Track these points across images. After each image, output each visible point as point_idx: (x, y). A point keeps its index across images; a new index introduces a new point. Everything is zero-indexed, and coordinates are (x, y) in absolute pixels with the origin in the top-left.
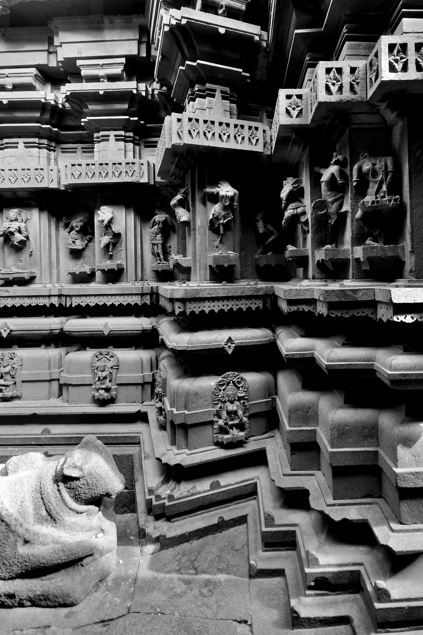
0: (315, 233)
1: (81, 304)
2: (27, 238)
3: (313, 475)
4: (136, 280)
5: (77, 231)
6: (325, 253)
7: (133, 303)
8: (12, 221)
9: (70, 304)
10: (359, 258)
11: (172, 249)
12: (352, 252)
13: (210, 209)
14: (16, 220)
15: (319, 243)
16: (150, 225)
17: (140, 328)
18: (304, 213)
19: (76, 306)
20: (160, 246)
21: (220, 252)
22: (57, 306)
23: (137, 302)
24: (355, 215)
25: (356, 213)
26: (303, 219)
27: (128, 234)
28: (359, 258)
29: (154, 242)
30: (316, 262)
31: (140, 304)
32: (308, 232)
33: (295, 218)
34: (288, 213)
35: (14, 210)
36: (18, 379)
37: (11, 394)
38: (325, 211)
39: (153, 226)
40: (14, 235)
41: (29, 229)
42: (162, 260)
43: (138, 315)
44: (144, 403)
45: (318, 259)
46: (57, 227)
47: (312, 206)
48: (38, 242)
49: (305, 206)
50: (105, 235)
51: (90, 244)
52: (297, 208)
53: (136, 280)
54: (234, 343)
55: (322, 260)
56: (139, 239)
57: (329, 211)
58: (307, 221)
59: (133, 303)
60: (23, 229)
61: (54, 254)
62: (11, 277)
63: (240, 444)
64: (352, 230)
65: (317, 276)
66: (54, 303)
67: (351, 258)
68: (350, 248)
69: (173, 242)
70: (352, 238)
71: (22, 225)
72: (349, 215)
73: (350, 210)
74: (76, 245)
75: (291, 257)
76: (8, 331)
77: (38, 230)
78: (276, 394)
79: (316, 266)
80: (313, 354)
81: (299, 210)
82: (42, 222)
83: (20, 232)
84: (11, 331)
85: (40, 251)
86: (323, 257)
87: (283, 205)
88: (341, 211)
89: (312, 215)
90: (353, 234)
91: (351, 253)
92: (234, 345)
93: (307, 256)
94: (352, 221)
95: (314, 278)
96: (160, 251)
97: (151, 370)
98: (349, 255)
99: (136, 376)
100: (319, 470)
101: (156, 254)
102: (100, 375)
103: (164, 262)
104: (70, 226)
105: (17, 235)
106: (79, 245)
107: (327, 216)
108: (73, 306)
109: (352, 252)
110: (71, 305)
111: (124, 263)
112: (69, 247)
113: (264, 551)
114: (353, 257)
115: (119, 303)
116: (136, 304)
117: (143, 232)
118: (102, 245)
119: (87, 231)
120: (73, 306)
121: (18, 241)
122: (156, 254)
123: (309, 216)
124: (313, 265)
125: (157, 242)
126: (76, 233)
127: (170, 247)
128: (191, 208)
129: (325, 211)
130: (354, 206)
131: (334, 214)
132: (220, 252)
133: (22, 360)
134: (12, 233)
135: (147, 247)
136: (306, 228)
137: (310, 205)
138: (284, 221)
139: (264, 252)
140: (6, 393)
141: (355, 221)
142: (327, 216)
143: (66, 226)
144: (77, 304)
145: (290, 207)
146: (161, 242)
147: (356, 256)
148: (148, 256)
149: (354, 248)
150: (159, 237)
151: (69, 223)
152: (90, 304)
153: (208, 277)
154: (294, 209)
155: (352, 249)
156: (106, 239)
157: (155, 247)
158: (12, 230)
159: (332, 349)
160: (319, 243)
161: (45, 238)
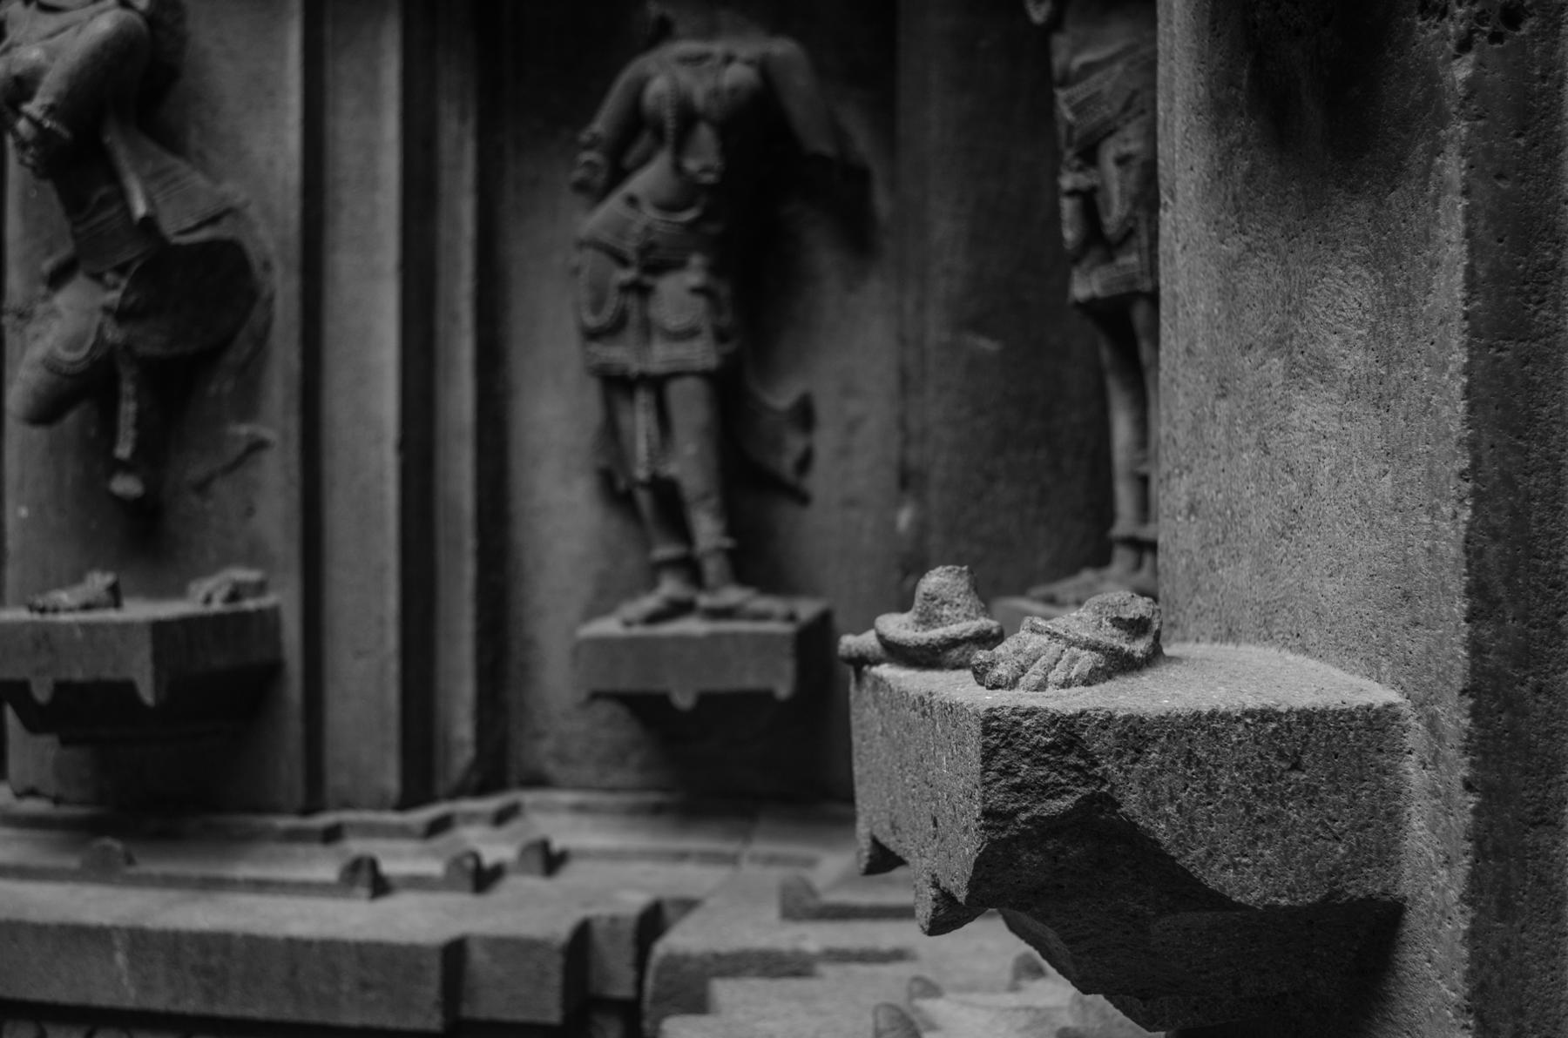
11: (825, 440)
20: (691, 407)
27: (343, 263)
29: (619, 354)
96: (689, 464)
103: (733, 595)
111: (284, 598)
125: (660, 357)
127: (804, 415)
150: (678, 295)
157: (640, 421)
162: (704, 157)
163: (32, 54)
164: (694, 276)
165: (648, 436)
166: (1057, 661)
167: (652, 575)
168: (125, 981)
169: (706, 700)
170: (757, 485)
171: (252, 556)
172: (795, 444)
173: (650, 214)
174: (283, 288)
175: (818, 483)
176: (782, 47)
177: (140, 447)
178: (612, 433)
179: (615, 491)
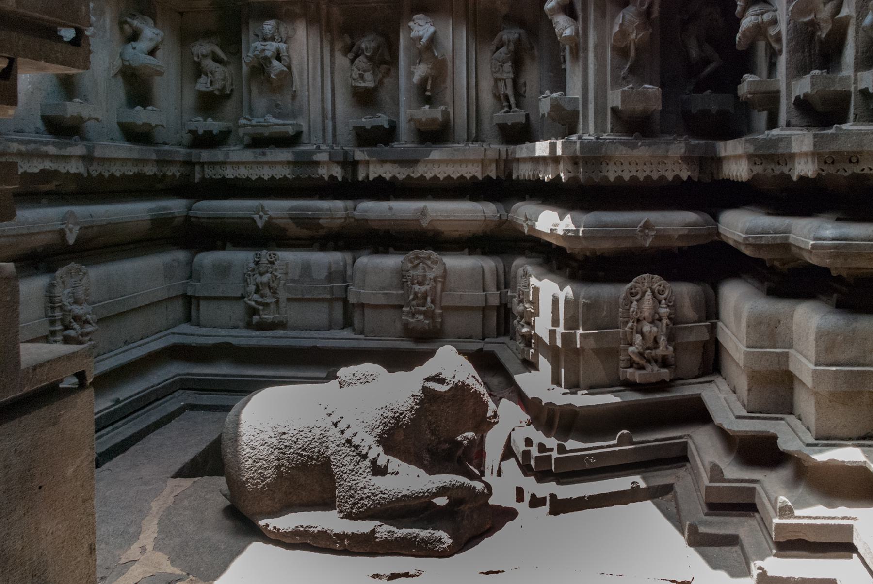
0: (792, 52)
1: (384, 176)
2: (289, 67)
3: (782, 419)
4: (468, 140)
5: (366, 57)
6: (812, 82)
7: (468, 176)
8: (265, 40)
9: (364, 175)
10: (867, 89)
11: (528, 88)
12: (856, 79)
13: (614, 17)
14: (273, 39)
15: (799, 70)
16: (493, 48)
17: (480, 216)
18: (774, 22)
19: (375, 179)
20: (509, 83)
21: (631, 86)
22: (340, 179)
23: (476, 174)
24: (862, 21)
25: (864, 19)
26: (772, 32)
27: (457, 61)
28: (867, 89)
29: (498, 75)
30: (793, 99)
31: (480, 178)
32: (781, 51)
33: (760, 30)
34: (746, 23)
35: (269, 22)
36: (283, 295)
37: (272, 317)
38: (812, 16)
39: (498, 49)
40: (270, 63)
41: (291, 53)
42: (513, 105)
43: (474, 198)
44: (486, 340)
45: (797, 94)
46: (332, 51)
47: (791, 8)
48: (305, 76)
49: (776, 10)
50: (419, 63)
51: (387, 81)
52: (762, 14)
53: (468, 140)
54: (653, 230)
55: (805, 95)
56: (473, 69)
57: (818, 17)
58: (779, 33)
59: (468, 176)
60: (284, 54)
61: (329, 95)
62: (266, 132)
63: (662, 386)
64: (857, 46)
65: (794, 121)
66: (335, 175)
67: (852, 89)
68: (852, 75)
69: (532, 75)
70: (856, 58)
71: (283, 46)
72: (853, 22)
73: (854, 14)
74: (364, 81)
75: (750, 93)
76: (265, 218)
77: (305, 56)
78: (718, 318)
79: (793, 106)
80: (787, 238)
81: (766, 17)
82: (311, 41)
83: (279, 58)
84: (270, 218)
85: (308, 90)
86: (808, 89)
87: (739, 8)
88: (839, 16)
89: (788, 23)
90: (857, 52)
91: (853, 81)
92: (653, 233)
93: (778, 92)
94: (857, 32)
95: (789, 125)
96: (510, 92)
97: (498, 289)
98: (850, 86)
99: (473, 296)
100: (791, 414)
101: (502, 97)
102: (416, 290)
103: (516, 109)
104: (354, 49)
105: (275, 63)
106: (369, 82)
107: (814, 25)
108: (371, 178)
109: (856, 79)
110: (367, 177)
111: (451, 110)
112: (354, 84)
113: (706, 515)
114: (855, 88)
115: (446, 175)
116: (474, 178)
117: (479, 58)
118: (416, 79)
119: (386, 59)
120: (371, 178)
121: (277, 71)
122: (502, 97)
123: (783, 27)
124: (787, 104)
125: (505, 76)
126: (365, 60)
127: (525, 84)
128: (580, 14)
129: (812, 16)
130: (861, 7)
131: (826, 21)
132: (631, 86)
133: (287, 264)
134: (267, 60)
135: (486, 85)
136: (776, 46)
137: (785, 8)
138: (738, 35)
139: (699, 89)
140: (263, 316)
141: (861, 31)
142: (814, 25)
143: (347, 50)
144: (376, 176)
145: (751, 11)
146: (511, 75)
147: (862, 86)
148: (487, 100)
149: (859, 73)
150: (508, 66)
151: (353, 45)
152: (398, 176)
153: (609, 126)
154: (758, 15)
155: (855, 75)
156: (421, 70)
157: (501, 85)
158: (268, 54)
159: (813, 428)
160: (799, 70)
161: (315, 68)
162: (512, 47)
163: (421, 33)
164: (510, 64)
165: (40, 19)
166: (174, 334)
167: (503, 108)
168: (626, 88)
169: (513, 124)
170: (519, 95)
171: (445, 104)
172: (524, 89)
173: (503, 55)
174: (450, 64)
175: (527, 95)
176: (522, 31)
177: (431, 87)
178: (496, 86)
179: (497, 97)
